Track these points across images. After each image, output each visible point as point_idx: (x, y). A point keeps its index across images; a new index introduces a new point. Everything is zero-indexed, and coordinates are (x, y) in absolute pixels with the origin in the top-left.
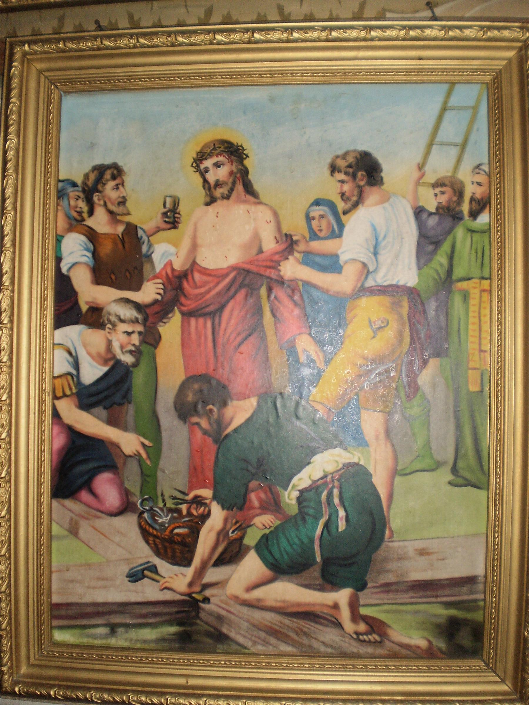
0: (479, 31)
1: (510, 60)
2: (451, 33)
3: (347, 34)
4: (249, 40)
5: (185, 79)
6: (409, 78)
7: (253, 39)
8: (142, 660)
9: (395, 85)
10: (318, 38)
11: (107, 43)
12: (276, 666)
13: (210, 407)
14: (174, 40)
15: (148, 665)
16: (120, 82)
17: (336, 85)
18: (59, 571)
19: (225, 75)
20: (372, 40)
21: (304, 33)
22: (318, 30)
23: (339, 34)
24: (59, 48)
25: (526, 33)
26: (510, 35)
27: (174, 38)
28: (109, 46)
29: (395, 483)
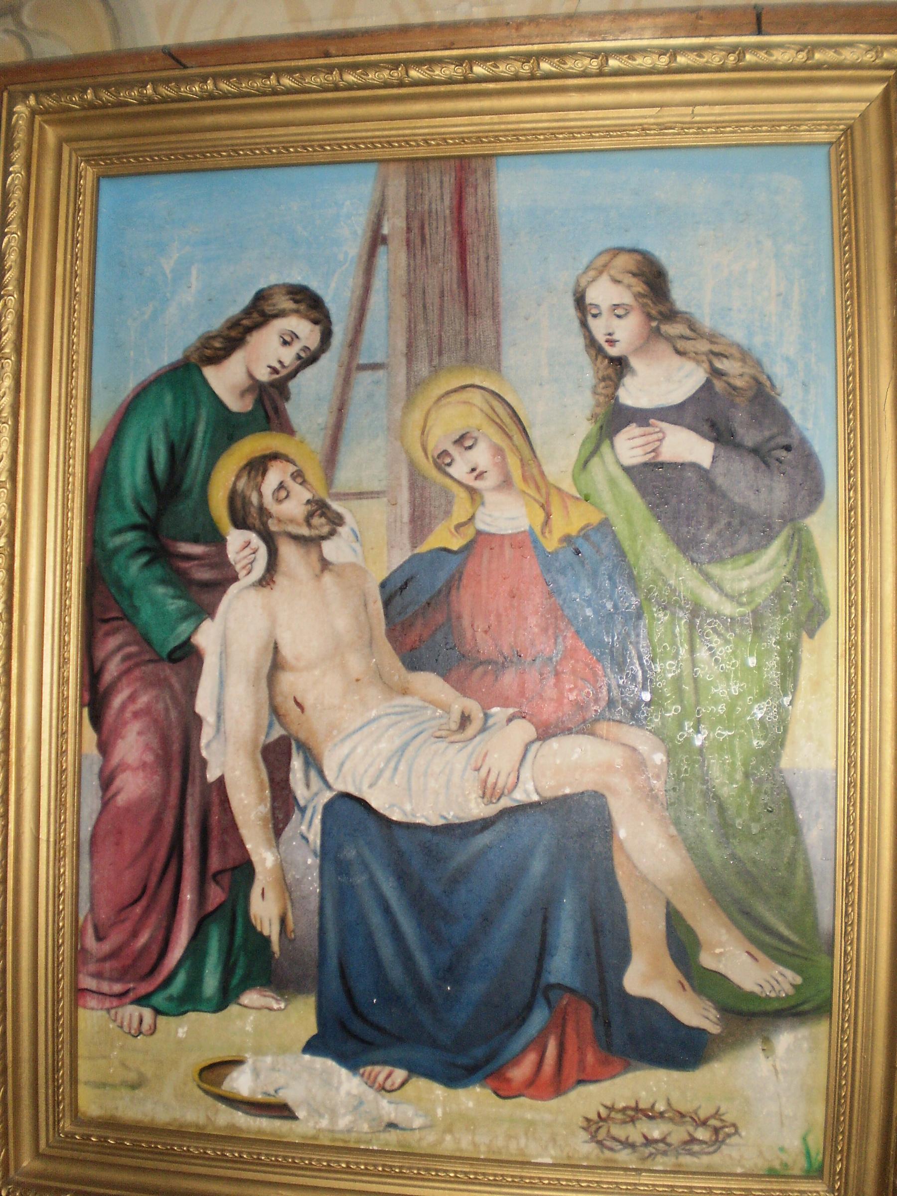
0: (867, 51)
1: (871, 101)
2: (818, 56)
3: (705, 60)
4: (465, 77)
5: (546, 139)
6: (668, 140)
7: (606, 69)
8: (348, 1167)
9: (750, 149)
10: (584, 71)
11: (224, 86)
12: (513, 1181)
13: (586, 690)
14: (338, 78)
15: (359, 1178)
16: (170, 159)
17: (589, 154)
18: (90, 1058)
19: (524, 135)
20: (818, 67)
21: (629, 58)
22: (654, 53)
23: (552, 66)
24: (86, 100)
25: (882, 53)
26: (855, 57)
27: (404, 72)
28: (230, 92)
29: (81, 1025)
